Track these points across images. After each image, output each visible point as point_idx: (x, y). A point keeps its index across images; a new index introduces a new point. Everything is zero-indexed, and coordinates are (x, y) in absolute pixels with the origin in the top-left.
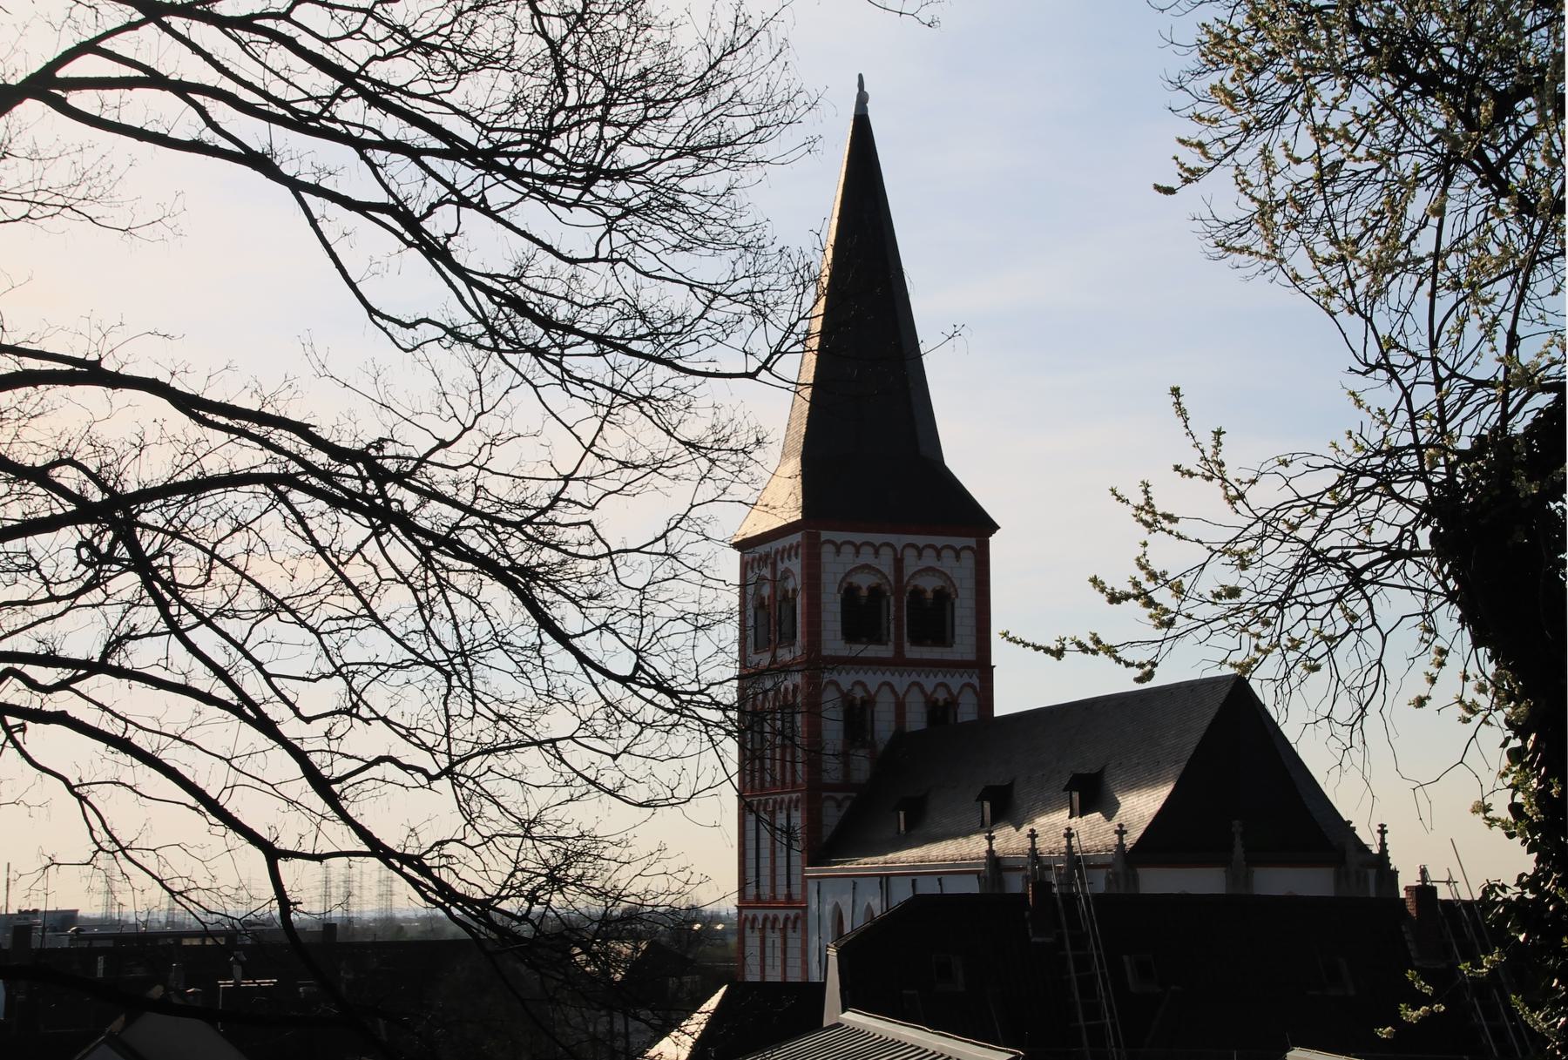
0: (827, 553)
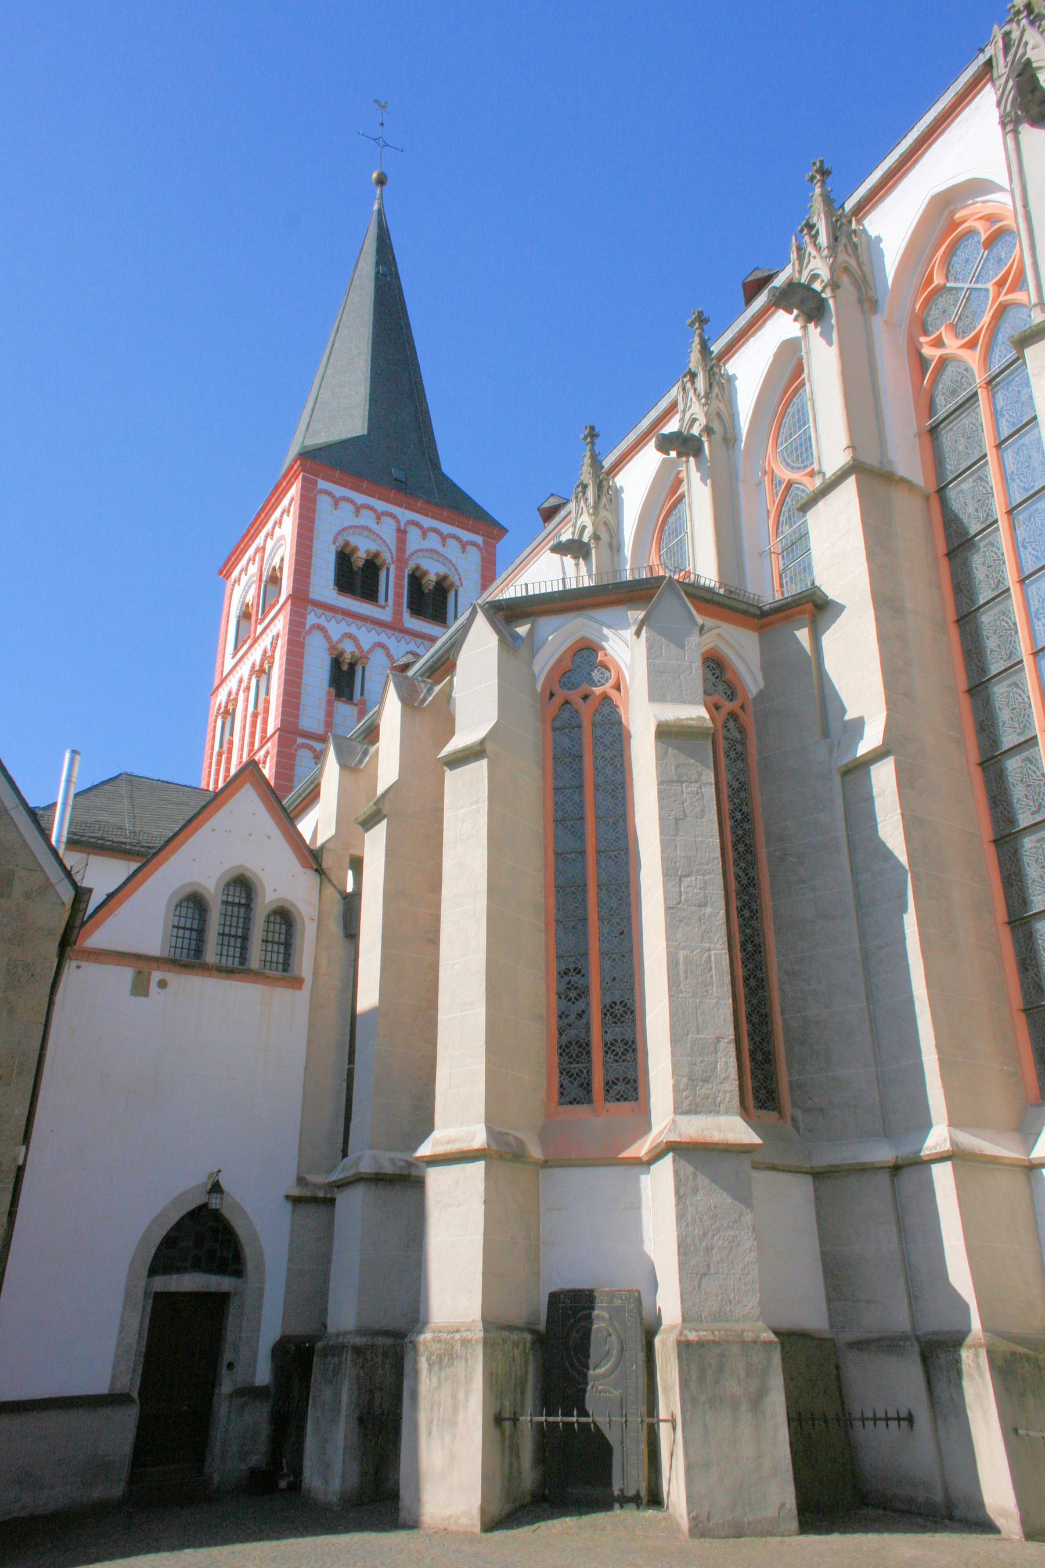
0: (323, 503)
